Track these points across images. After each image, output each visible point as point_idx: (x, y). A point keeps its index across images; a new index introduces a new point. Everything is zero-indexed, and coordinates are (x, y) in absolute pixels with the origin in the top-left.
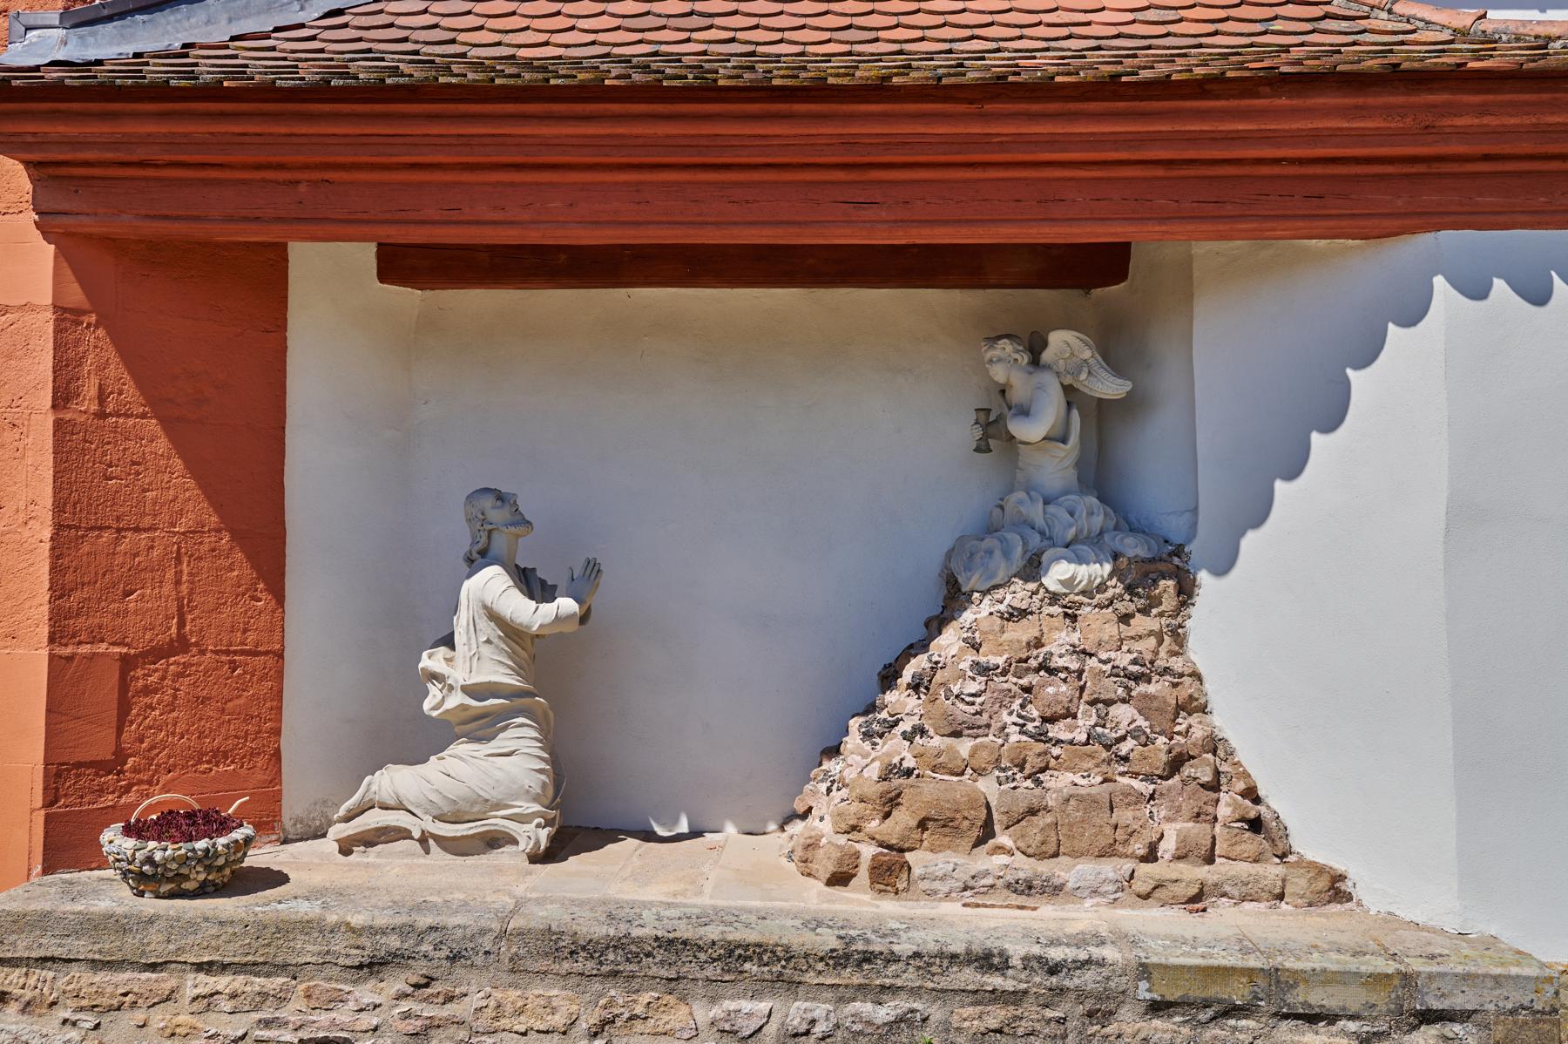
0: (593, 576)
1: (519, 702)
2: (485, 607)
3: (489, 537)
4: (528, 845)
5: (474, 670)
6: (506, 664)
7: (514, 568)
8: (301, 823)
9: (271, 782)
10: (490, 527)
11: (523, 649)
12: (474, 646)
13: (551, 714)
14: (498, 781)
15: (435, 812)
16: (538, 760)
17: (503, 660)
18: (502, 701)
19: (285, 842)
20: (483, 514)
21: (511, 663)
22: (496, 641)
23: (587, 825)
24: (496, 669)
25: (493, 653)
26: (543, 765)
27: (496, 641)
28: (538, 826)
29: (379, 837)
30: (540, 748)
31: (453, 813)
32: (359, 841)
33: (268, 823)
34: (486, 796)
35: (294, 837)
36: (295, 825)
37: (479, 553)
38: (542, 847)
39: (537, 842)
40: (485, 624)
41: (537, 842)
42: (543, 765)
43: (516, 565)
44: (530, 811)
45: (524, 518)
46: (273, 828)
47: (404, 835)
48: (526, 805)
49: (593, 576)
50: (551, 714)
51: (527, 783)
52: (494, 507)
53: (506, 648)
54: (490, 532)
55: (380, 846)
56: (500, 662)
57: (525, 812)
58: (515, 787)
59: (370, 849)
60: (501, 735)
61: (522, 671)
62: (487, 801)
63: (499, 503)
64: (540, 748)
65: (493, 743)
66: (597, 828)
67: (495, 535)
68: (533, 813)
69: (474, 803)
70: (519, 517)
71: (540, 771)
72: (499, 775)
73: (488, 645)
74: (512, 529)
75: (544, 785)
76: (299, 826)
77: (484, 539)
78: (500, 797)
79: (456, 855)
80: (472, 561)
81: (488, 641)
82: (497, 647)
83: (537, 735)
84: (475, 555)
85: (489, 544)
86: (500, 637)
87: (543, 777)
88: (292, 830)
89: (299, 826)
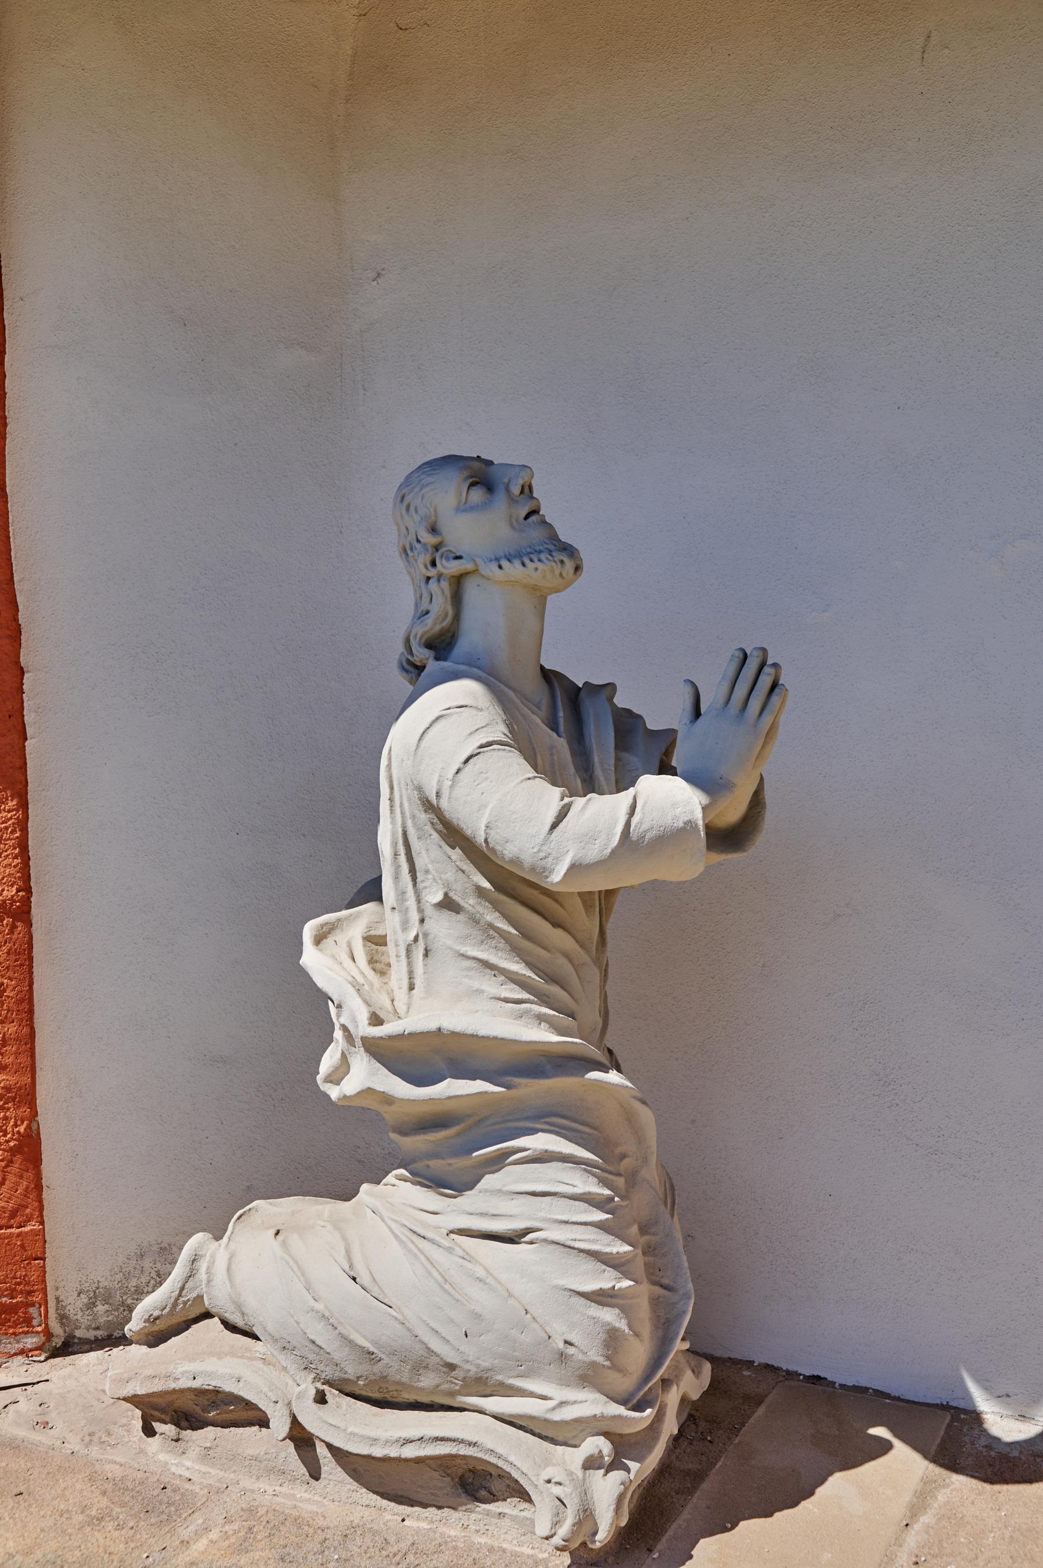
0: (755, 704)
1: (531, 1089)
2: (429, 806)
3: (457, 598)
4: (556, 1524)
5: (418, 982)
6: (503, 972)
7: (534, 685)
8: (106, 1302)
9: (13, 1214)
10: (453, 567)
11: (556, 925)
12: (415, 917)
13: (646, 1116)
14: (477, 1316)
15: (329, 1373)
16: (592, 1265)
17: (493, 959)
18: (480, 1086)
19: (67, 1348)
20: (434, 530)
21: (517, 967)
22: (470, 902)
23: (792, 1367)
24: (476, 984)
25: (465, 938)
26: (607, 1280)
27: (470, 902)
28: (591, 1463)
29: (206, 1410)
30: (599, 1226)
31: (370, 1383)
32: (163, 1411)
33: (13, 1309)
34: (452, 1358)
35: (91, 1335)
36: (91, 1305)
37: (429, 645)
38: (603, 1535)
39: (587, 1516)
40: (436, 853)
41: (587, 1516)
42: (607, 1280)
43: (548, 676)
44: (568, 1414)
45: (554, 537)
46: (28, 1321)
47: (251, 1414)
48: (559, 1393)
49: (755, 704)
50: (646, 1116)
51: (560, 1331)
52: (463, 508)
53: (503, 925)
54: (458, 582)
55: (210, 1431)
56: (486, 965)
57: (557, 1416)
58: (526, 1338)
59: (187, 1434)
60: (489, 1181)
61: (555, 990)
62: (452, 1367)
63: (477, 495)
64: (599, 1226)
65: (469, 1199)
66: (816, 1379)
67: (472, 592)
68: (577, 1421)
69: (420, 1366)
70: (535, 535)
71: (600, 1298)
72: (480, 1299)
73: (446, 914)
74: (514, 570)
75: (612, 1339)
76: (101, 1308)
77: (440, 603)
78: (485, 1364)
79: (384, 1496)
80: (420, 669)
81: (448, 904)
82: (475, 920)
83: (593, 1187)
84: (421, 654)
85: (457, 617)
86: (480, 892)
87: (609, 1316)
88: (84, 1319)
89: (101, 1308)
